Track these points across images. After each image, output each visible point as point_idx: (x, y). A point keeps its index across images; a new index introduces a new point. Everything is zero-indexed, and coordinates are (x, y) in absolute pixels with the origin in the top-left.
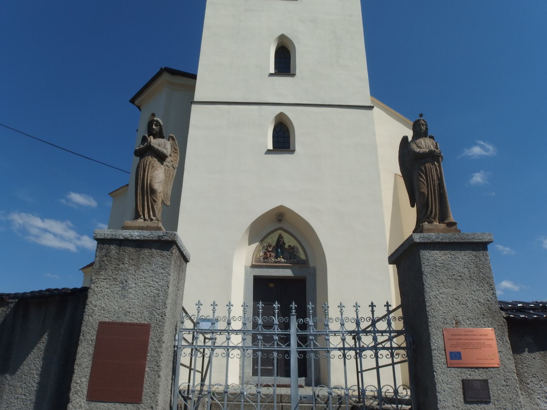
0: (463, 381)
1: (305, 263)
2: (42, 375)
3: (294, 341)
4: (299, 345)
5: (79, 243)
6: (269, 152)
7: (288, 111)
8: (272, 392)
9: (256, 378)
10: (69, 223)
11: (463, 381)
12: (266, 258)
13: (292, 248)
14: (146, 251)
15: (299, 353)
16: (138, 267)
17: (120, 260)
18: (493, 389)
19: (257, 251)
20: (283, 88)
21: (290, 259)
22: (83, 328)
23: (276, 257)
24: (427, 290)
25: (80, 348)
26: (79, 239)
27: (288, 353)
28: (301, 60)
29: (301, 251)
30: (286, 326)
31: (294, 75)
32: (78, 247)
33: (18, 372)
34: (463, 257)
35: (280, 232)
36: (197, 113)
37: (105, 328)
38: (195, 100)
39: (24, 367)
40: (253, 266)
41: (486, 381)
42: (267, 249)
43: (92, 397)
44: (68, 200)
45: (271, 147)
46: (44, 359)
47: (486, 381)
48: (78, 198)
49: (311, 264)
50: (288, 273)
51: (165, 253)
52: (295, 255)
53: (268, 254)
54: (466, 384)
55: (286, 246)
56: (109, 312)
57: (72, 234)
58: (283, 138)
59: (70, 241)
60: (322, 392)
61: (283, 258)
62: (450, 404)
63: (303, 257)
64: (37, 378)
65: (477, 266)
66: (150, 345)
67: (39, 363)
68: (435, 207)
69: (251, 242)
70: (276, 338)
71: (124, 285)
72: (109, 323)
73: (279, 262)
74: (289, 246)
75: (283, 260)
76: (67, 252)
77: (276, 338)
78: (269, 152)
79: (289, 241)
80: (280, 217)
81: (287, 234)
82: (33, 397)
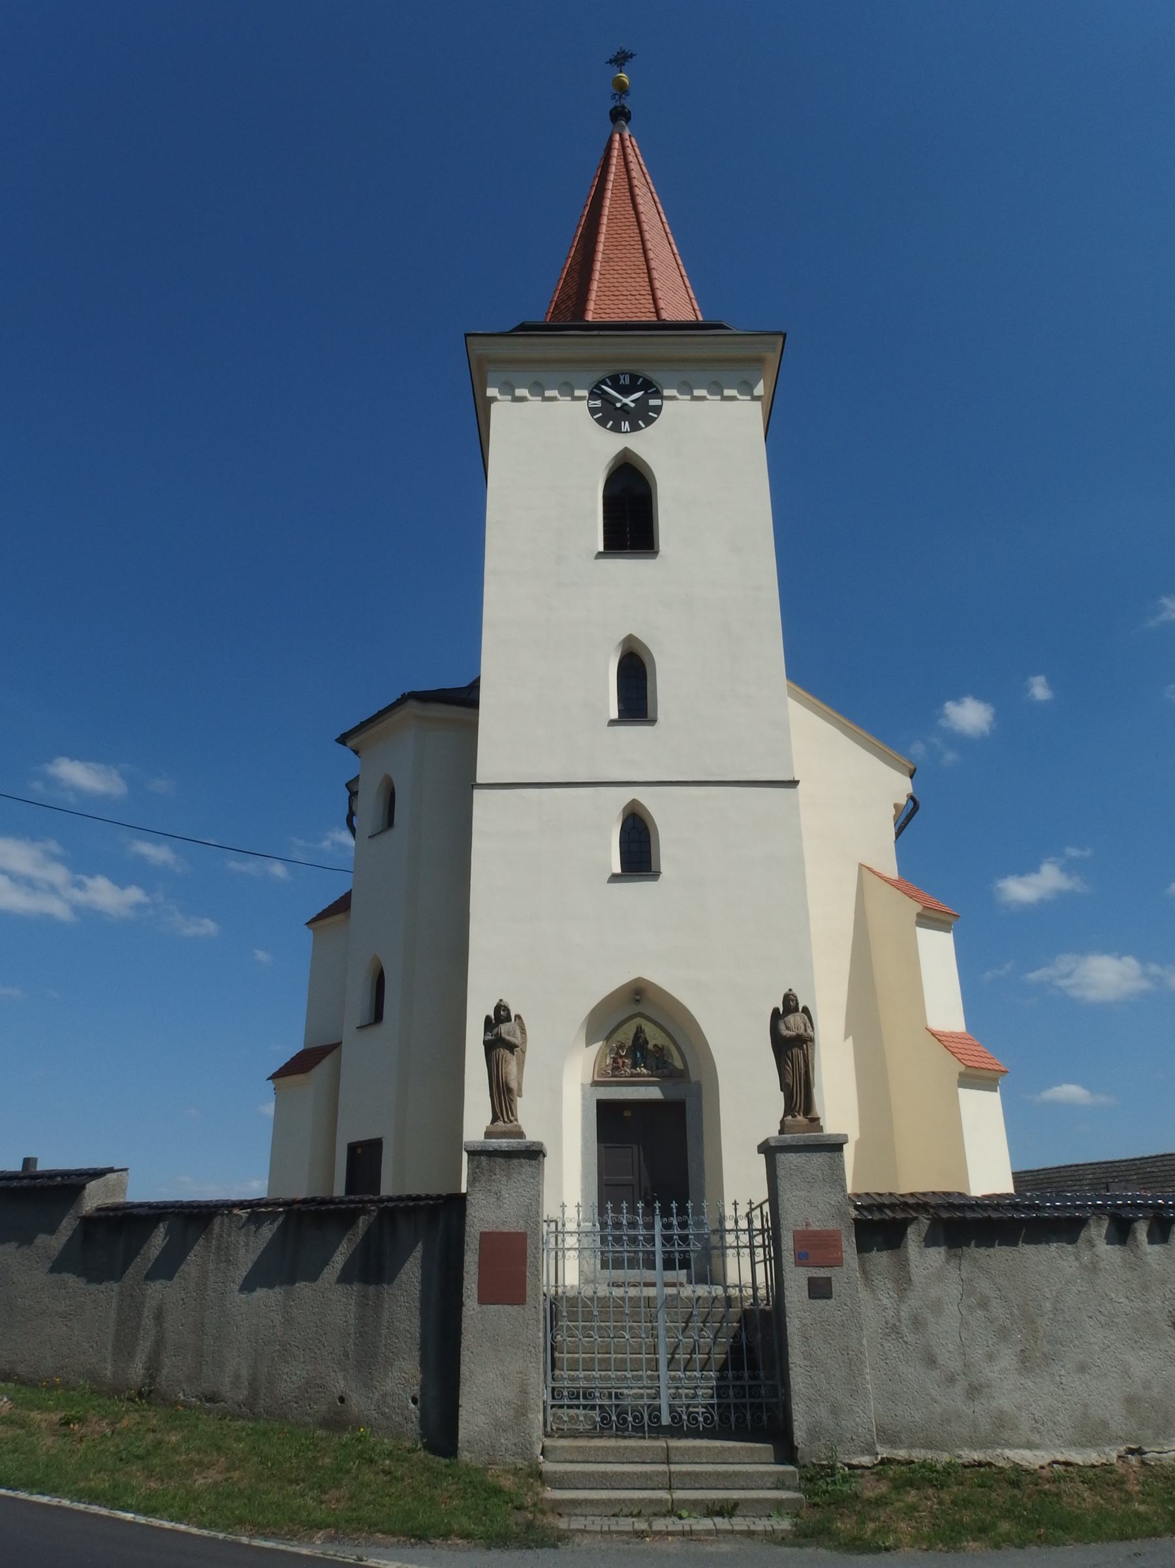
0: (809, 1279)
1: (681, 1075)
2: (423, 1283)
3: (658, 1240)
4: (663, 1245)
5: (79, 896)
6: (614, 878)
7: (643, 796)
8: (639, 1294)
9: (606, 1272)
10: (53, 846)
11: (809, 1279)
12: (616, 1068)
13: (660, 1049)
14: (515, 1161)
15: (664, 1252)
16: (509, 1177)
17: (492, 1171)
18: (836, 1287)
19: (601, 1056)
20: (635, 751)
21: (658, 1068)
22: (466, 1239)
23: (634, 1066)
24: (780, 1193)
25: (466, 1258)
26: (81, 886)
27: (654, 1253)
28: (668, 687)
29: (675, 1053)
30: (650, 1226)
31: (653, 722)
32: (76, 909)
33: (396, 1281)
34: (819, 1158)
35: (638, 1021)
36: (486, 810)
37: (485, 1237)
38: (479, 781)
39: (403, 1276)
40: (595, 1084)
41: (829, 1279)
42: (618, 1053)
43: (483, 1300)
44: (52, 782)
45: (617, 869)
46: (422, 1267)
47: (829, 1279)
48: (77, 775)
49: (693, 1077)
50: (654, 1093)
51: (533, 1162)
52: (665, 1062)
53: (620, 1061)
54: (812, 1282)
55: (650, 1046)
56: (488, 1223)
57: (57, 874)
58: (638, 851)
59: (53, 889)
60: (718, 1291)
61: (645, 1067)
62: (796, 1299)
63: (678, 1063)
64: (418, 1286)
65: (830, 1168)
66: (529, 1252)
67: (418, 1273)
68: (799, 1100)
69: (589, 1043)
70: (641, 1238)
71: (498, 1196)
72: (489, 1233)
73: (639, 1075)
74: (655, 1046)
75: (644, 1071)
76: (45, 922)
77: (641, 1238)
78: (614, 878)
79: (654, 1036)
80: (638, 994)
81: (650, 1024)
82: (417, 1304)
